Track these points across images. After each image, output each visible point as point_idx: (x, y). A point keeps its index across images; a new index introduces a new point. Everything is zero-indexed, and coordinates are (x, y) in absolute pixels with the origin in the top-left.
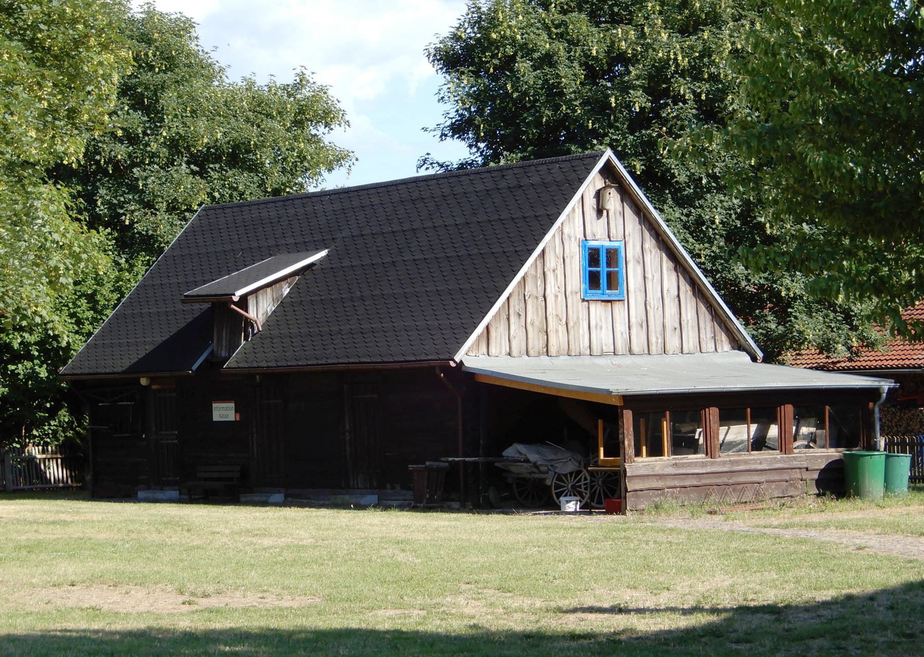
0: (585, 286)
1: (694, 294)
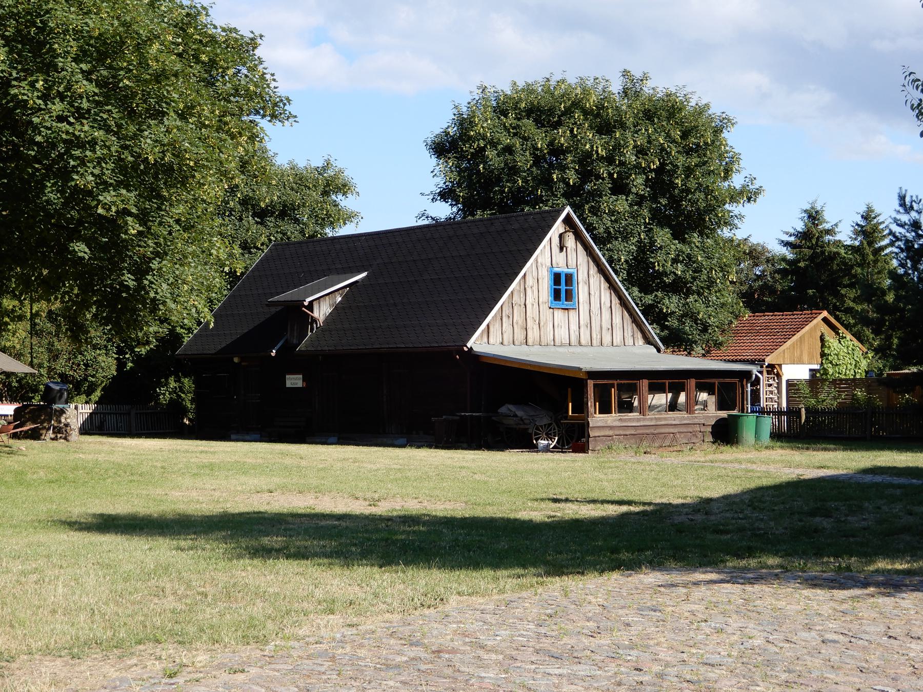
0: (551, 298)
1: (621, 304)
